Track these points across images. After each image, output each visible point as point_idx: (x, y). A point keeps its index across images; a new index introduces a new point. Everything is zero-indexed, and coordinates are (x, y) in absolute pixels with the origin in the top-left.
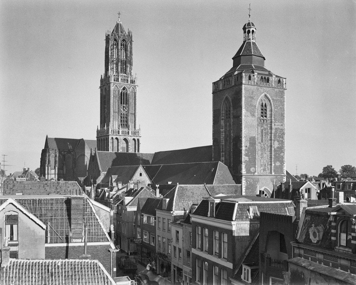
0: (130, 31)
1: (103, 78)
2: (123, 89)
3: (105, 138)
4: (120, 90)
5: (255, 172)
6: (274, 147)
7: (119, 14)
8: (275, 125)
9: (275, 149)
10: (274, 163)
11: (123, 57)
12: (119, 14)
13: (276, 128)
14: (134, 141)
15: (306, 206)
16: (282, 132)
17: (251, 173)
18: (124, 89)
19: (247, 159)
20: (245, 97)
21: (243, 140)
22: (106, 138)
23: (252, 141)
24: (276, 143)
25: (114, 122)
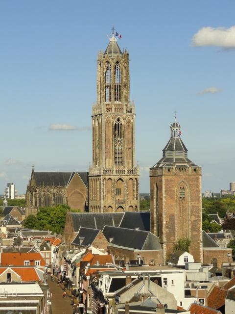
7: (175, 112)
9: (192, 223)
11: (117, 82)
13: (193, 206)
15: (120, 266)
21: (164, 216)
23: (172, 217)
24: (193, 217)
25: (107, 159)
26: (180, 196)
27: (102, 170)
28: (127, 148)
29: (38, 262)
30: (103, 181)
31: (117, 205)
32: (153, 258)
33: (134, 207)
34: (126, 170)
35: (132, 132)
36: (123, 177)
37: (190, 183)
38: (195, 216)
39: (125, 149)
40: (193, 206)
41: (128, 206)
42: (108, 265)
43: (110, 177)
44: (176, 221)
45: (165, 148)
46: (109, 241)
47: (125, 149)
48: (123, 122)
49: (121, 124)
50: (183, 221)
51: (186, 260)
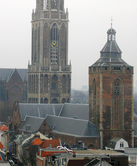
1: (34, 13)
2: (53, 25)
3: (35, 75)
4: (50, 26)
5: (110, 128)
6: (124, 112)
8: (125, 97)
13: (126, 100)
16: (130, 102)
18: (54, 25)
20: (102, 81)
22: (37, 75)
24: (126, 109)
26: (115, 91)
31: (52, 98)
32: (91, 144)
33: (66, 99)
34: (60, 68)
39: (60, 50)
40: (126, 100)
41: (61, 99)
42: (59, 148)
44: (111, 112)
45: (108, 31)
48: (59, 27)
50: (117, 112)
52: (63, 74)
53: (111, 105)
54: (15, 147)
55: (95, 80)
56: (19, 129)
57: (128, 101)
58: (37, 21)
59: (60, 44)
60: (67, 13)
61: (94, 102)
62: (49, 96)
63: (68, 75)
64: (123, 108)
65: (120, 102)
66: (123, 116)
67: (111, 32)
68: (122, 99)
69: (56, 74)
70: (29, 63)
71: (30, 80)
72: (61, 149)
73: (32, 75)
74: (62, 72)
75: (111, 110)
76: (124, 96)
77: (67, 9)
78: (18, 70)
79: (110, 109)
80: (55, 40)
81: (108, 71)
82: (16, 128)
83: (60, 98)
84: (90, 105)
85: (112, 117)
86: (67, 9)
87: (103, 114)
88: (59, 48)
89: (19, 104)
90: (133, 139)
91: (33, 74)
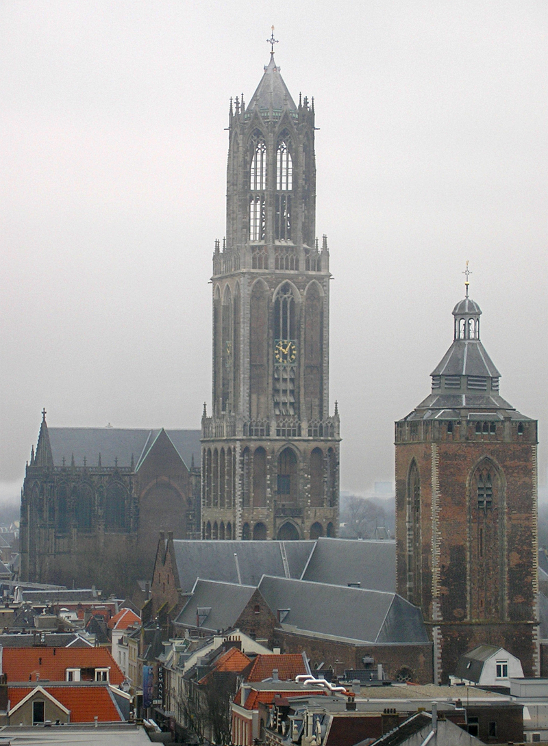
0: (306, 99)
1: (221, 251)
2: (282, 290)
3: (226, 450)
4: (272, 293)
5: (465, 616)
6: (509, 565)
7: (467, 273)
8: (510, 518)
10: (509, 599)
12: (272, 41)
13: (514, 526)
14: (118, 653)
16: (529, 533)
17: (455, 619)
18: (285, 289)
19: (445, 592)
20: (439, 467)
25: (254, 397)
26: (481, 499)
27: (240, 427)
28: (307, 367)
29: (105, 674)
30: (242, 455)
33: (325, 526)
35: (322, 322)
36: (295, 443)
37: (508, 463)
38: (519, 552)
39: (302, 369)
40: (514, 526)
42: (301, 679)
43: (263, 444)
44: (468, 566)
45: (455, 309)
46: (150, 603)
47: (302, 369)
48: (300, 296)
49: (293, 301)
50: (487, 564)
51: (502, 671)
52: (313, 445)
53: (468, 544)
54: (163, 677)
55: (415, 465)
56: (174, 622)
57: (520, 529)
58: (229, 279)
59: (302, 351)
60: (326, 252)
61: (412, 533)
62: (268, 516)
63: (330, 449)
64: (506, 553)
65: (495, 533)
66: (506, 577)
67: (466, 312)
68: (503, 525)
69: (292, 447)
70: (205, 412)
71: (209, 465)
72: (309, 683)
73: (216, 450)
74: (311, 438)
75: (468, 560)
76: (508, 513)
77: (325, 238)
78: (170, 432)
79: (465, 556)
80: (288, 337)
81: (457, 435)
82: (164, 617)
83: (303, 523)
84: (400, 545)
85: (470, 580)
86: (325, 238)
87: (442, 573)
88: (299, 364)
89: (174, 540)
90: (536, 651)
91: (219, 446)
